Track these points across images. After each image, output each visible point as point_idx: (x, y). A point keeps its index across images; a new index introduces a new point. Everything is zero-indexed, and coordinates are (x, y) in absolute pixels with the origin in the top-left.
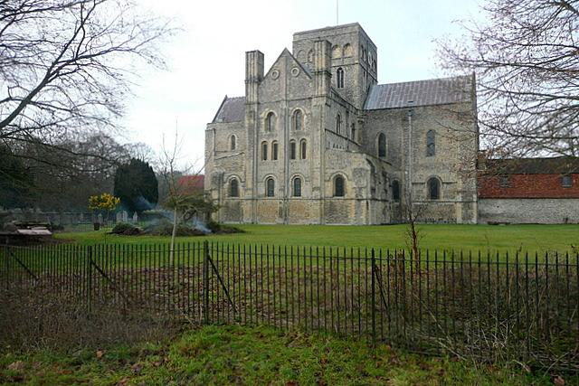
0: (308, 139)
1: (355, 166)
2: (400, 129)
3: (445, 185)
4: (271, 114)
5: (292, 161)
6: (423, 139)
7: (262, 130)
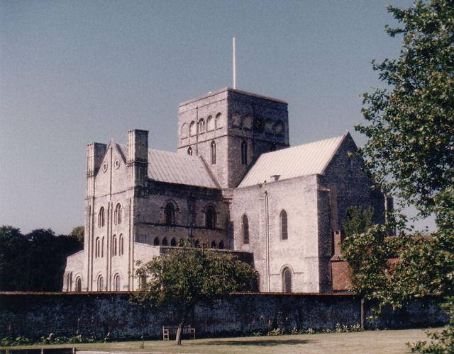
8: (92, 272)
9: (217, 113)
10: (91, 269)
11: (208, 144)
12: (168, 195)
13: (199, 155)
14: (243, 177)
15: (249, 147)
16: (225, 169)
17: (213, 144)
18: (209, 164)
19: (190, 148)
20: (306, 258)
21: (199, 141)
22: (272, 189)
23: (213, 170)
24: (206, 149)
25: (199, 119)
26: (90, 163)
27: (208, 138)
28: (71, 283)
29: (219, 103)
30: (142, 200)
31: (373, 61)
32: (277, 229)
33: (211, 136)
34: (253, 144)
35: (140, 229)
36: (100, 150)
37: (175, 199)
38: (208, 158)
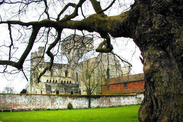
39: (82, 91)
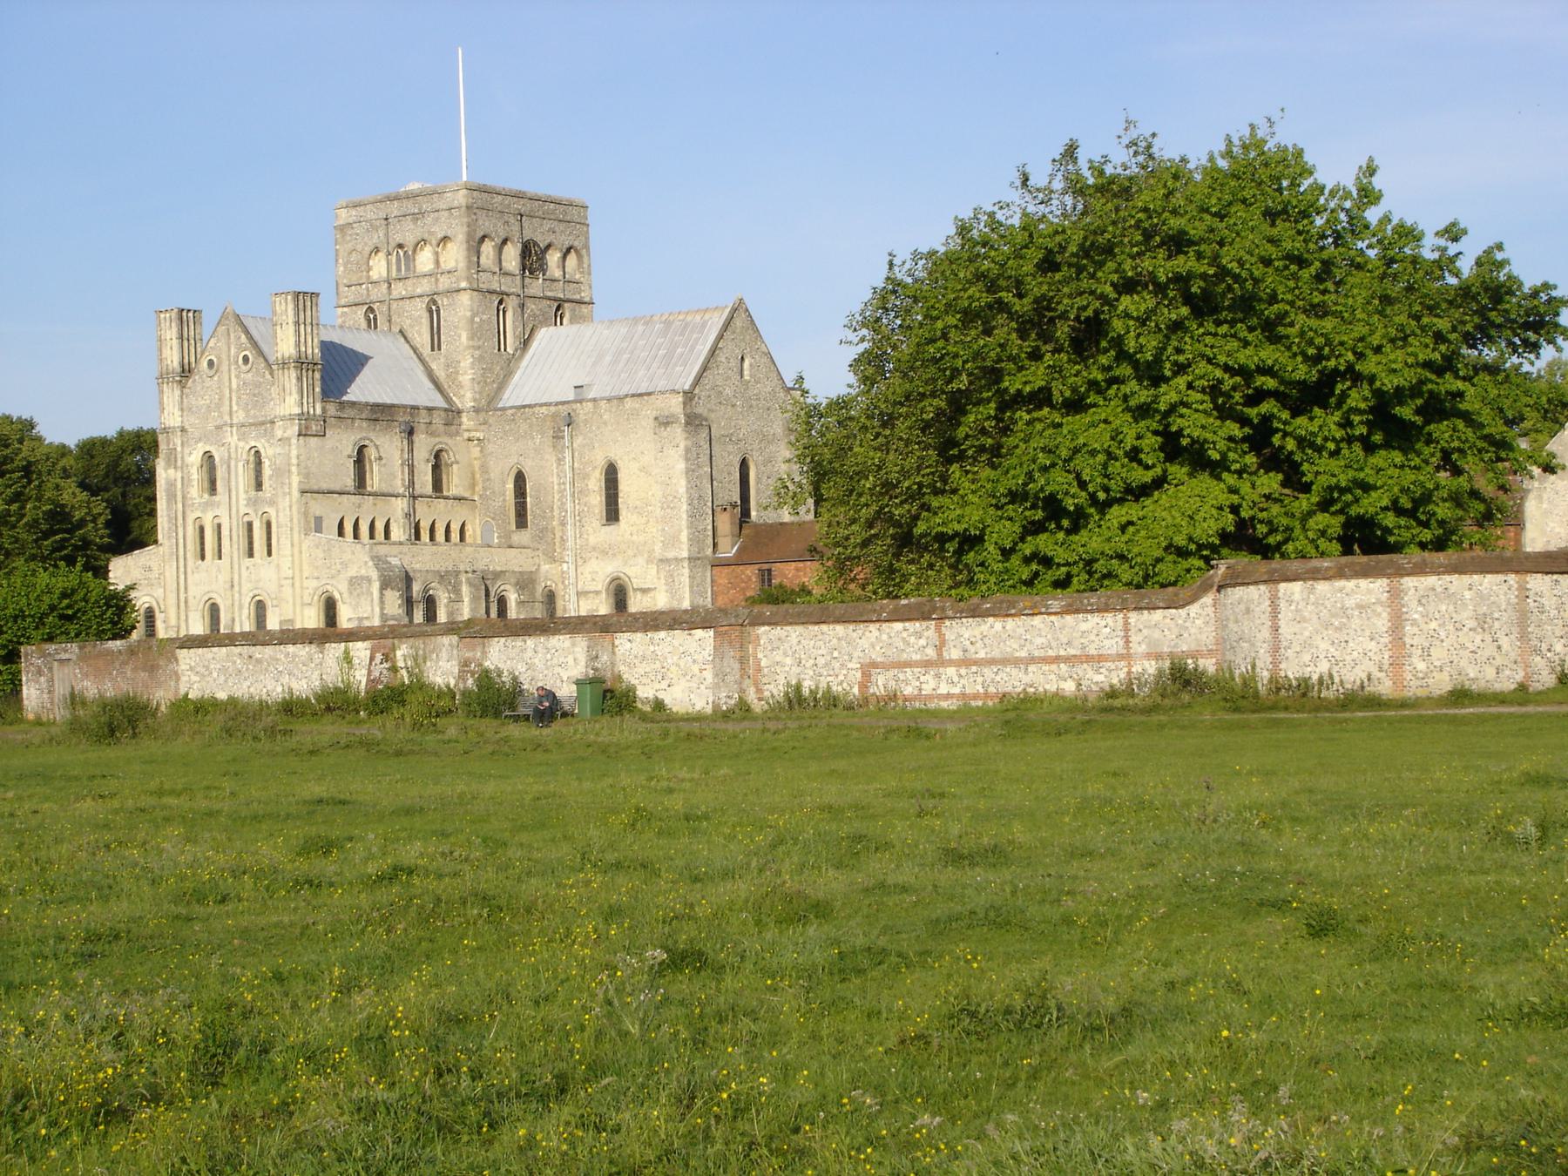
0: (272, 512)
1: (352, 572)
2: (550, 457)
3: (639, 595)
4: (208, 457)
5: (248, 561)
6: (596, 483)
7: (194, 492)
8: (186, 592)
9: (440, 236)
10: (182, 587)
11: (420, 306)
12: (360, 427)
13: (396, 329)
14: (502, 386)
15: (509, 315)
16: (466, 362)
17: (433, 310)
18: (426, 351)
19: (371, 309)
20: (661, 560)
21: (395, 294)
22: (679, 430)
23: (434, 366)
24: (415, 319)
25: (393, 244)
26: (167, 352)
27: (419, 291)
28: (1520, 704)
29: (446, 214)
30: (313, 441)
31: (1025, 180)
32: (597, 500)
33: (425, 287)
34: (522, 306)
35: (312, 503)
36: (186, 318)
37: (372, 435)
38: (422, 338)
39: (572, 591)
